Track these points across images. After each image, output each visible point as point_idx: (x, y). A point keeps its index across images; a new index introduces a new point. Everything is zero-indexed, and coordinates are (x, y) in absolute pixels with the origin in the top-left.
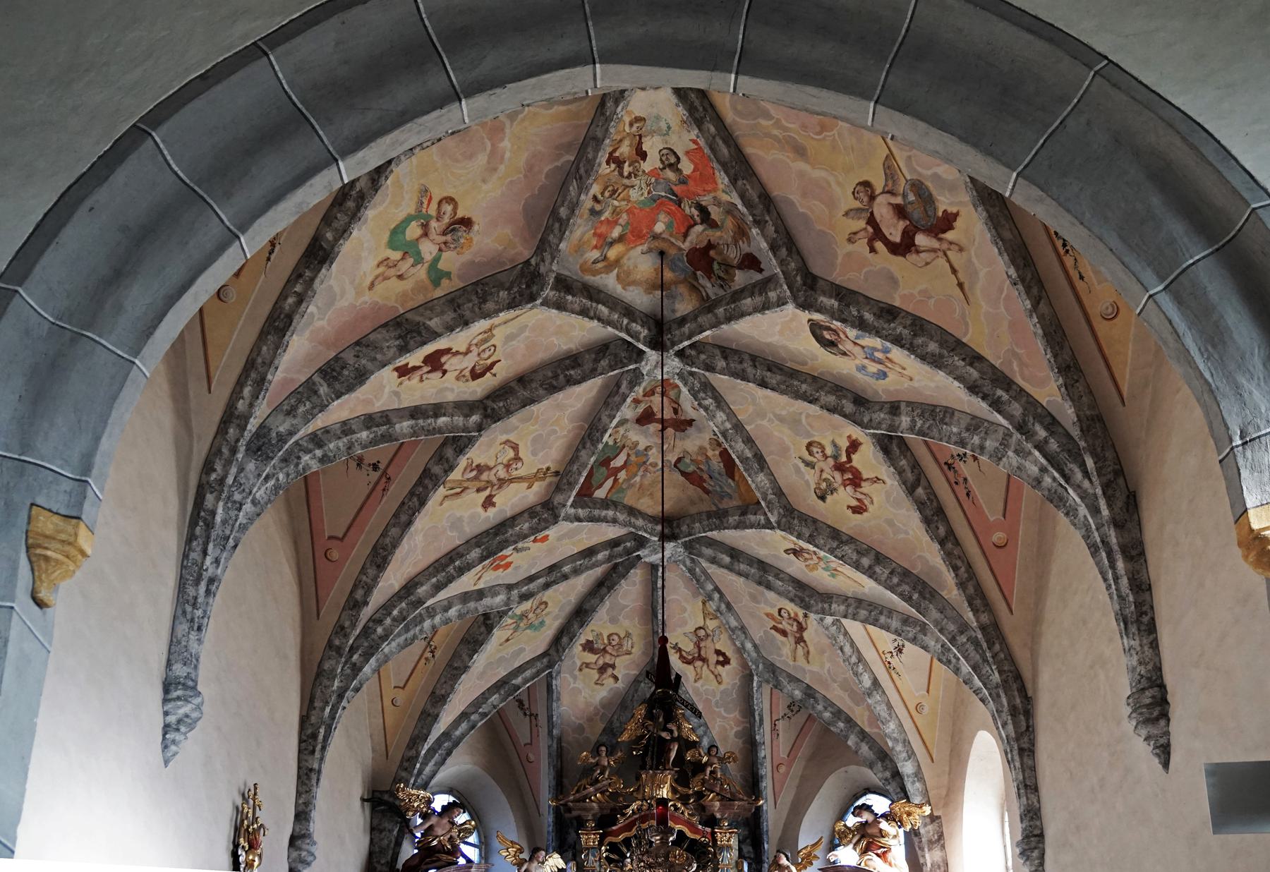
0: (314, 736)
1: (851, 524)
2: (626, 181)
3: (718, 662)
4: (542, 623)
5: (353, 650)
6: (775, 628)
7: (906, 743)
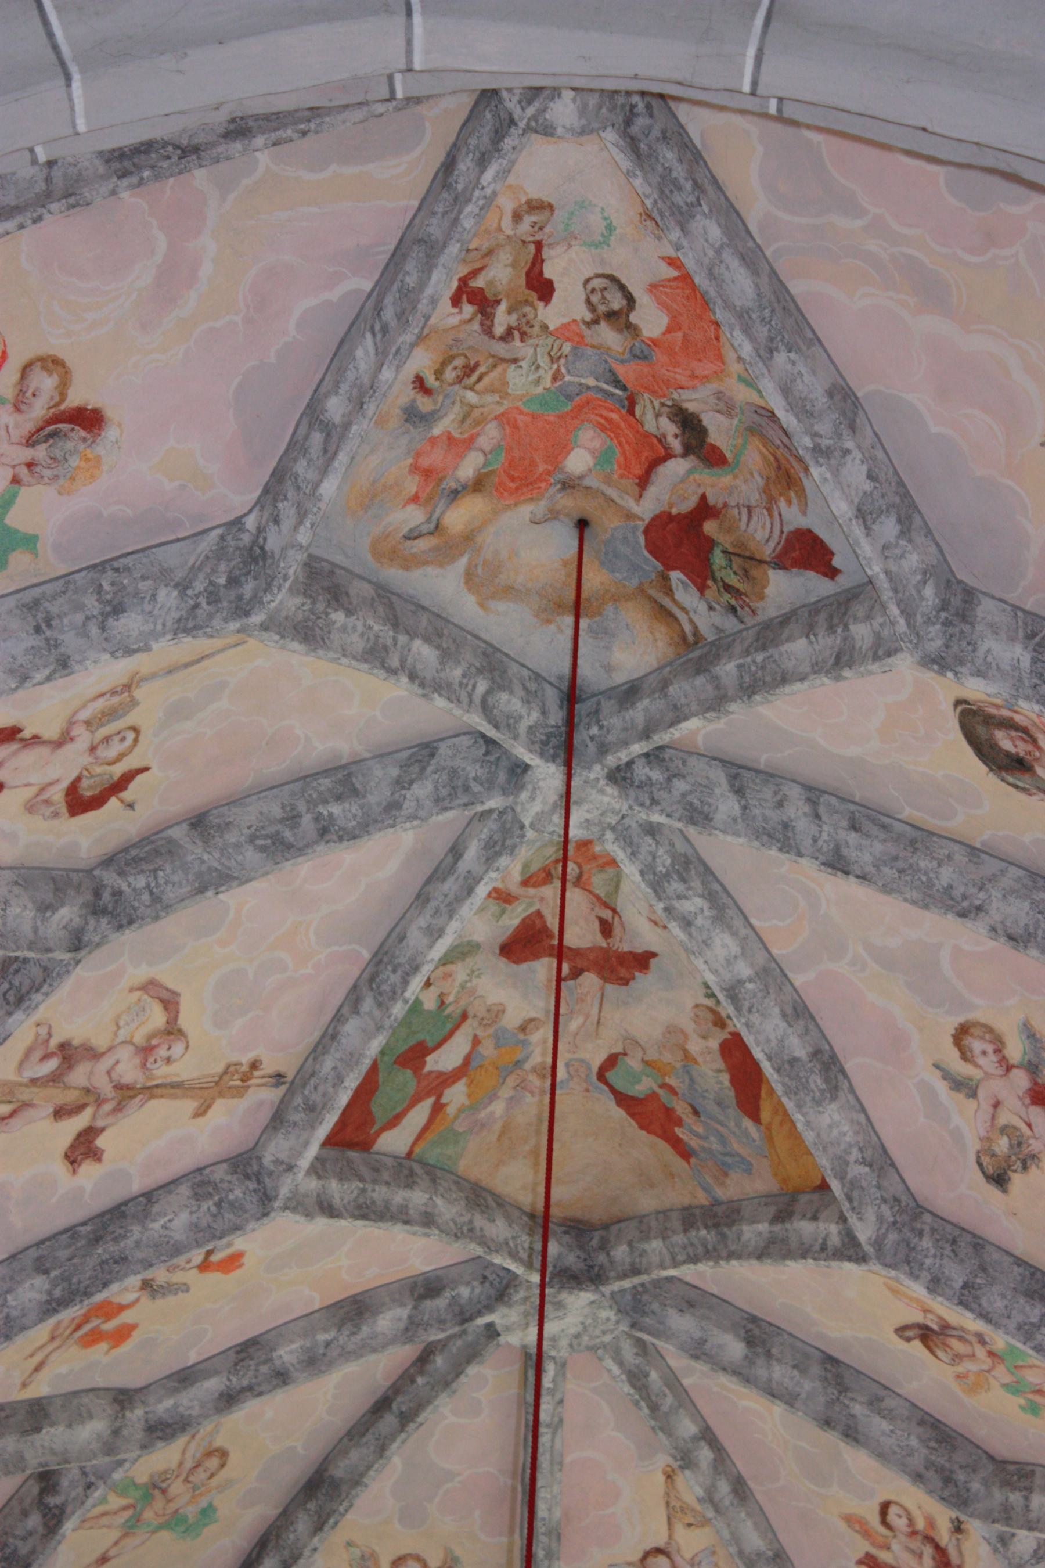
2: (501, 349)
4: (208, 1513)
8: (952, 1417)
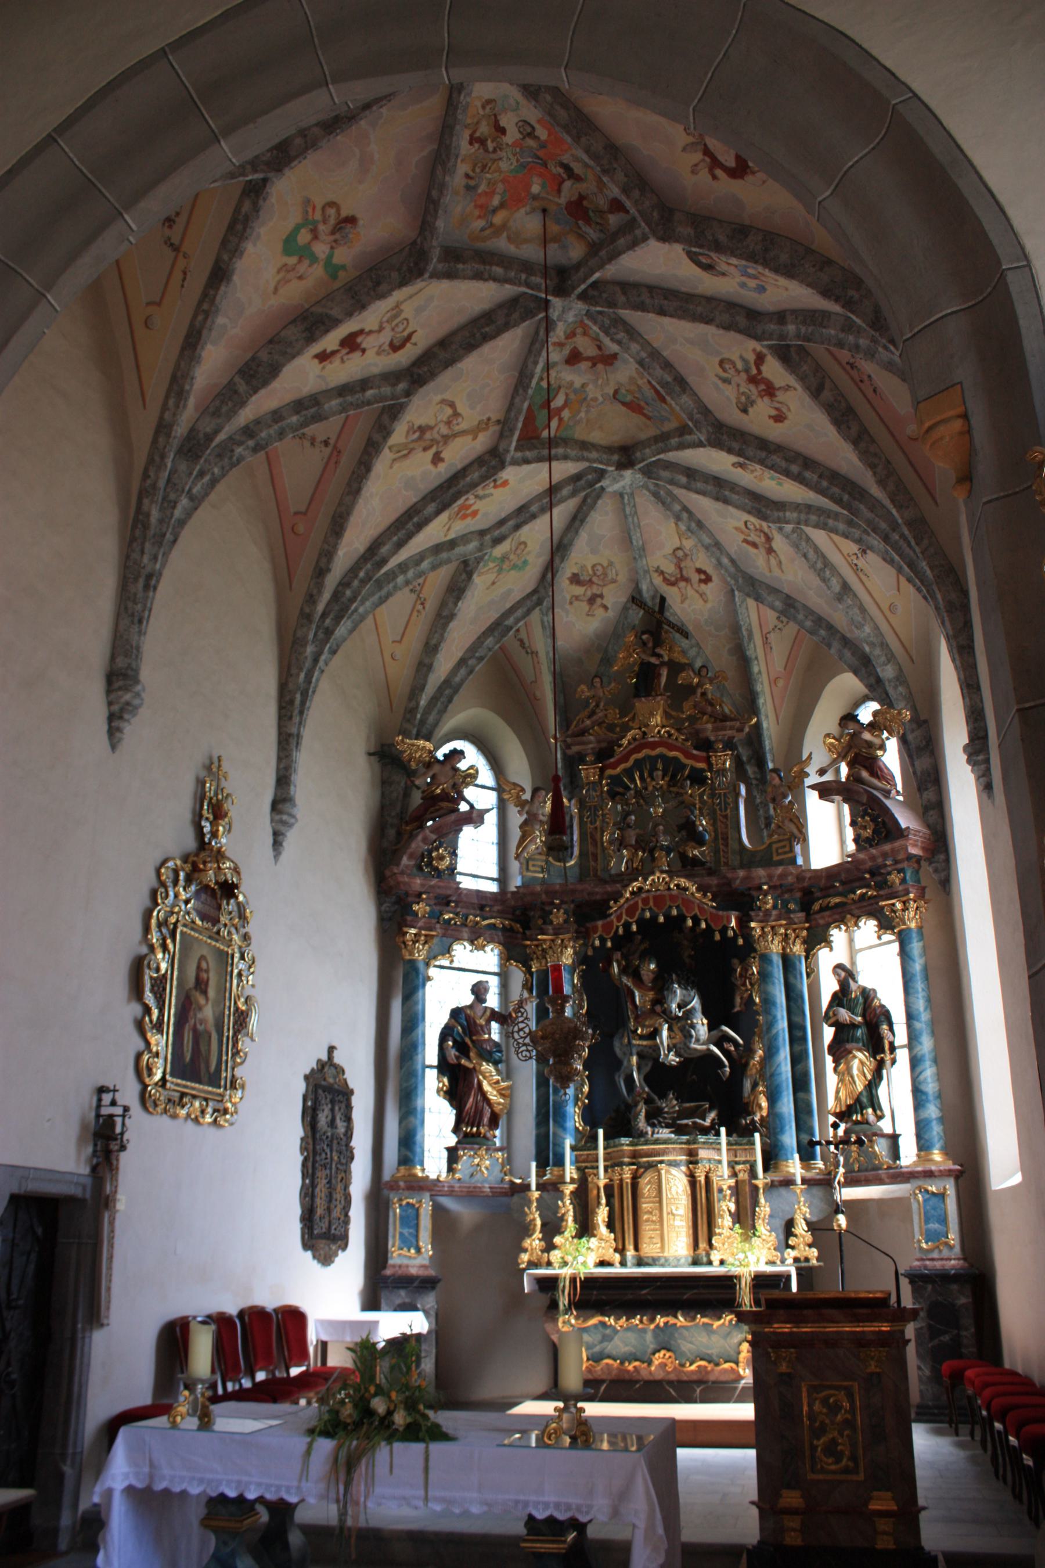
0: (292, 702)
1: (775, 432)
3: (701, 581)
4: (525, 562)
5: (324, 615)
6: (745, 541)
7: (884, 645)
8: (758, 491)
